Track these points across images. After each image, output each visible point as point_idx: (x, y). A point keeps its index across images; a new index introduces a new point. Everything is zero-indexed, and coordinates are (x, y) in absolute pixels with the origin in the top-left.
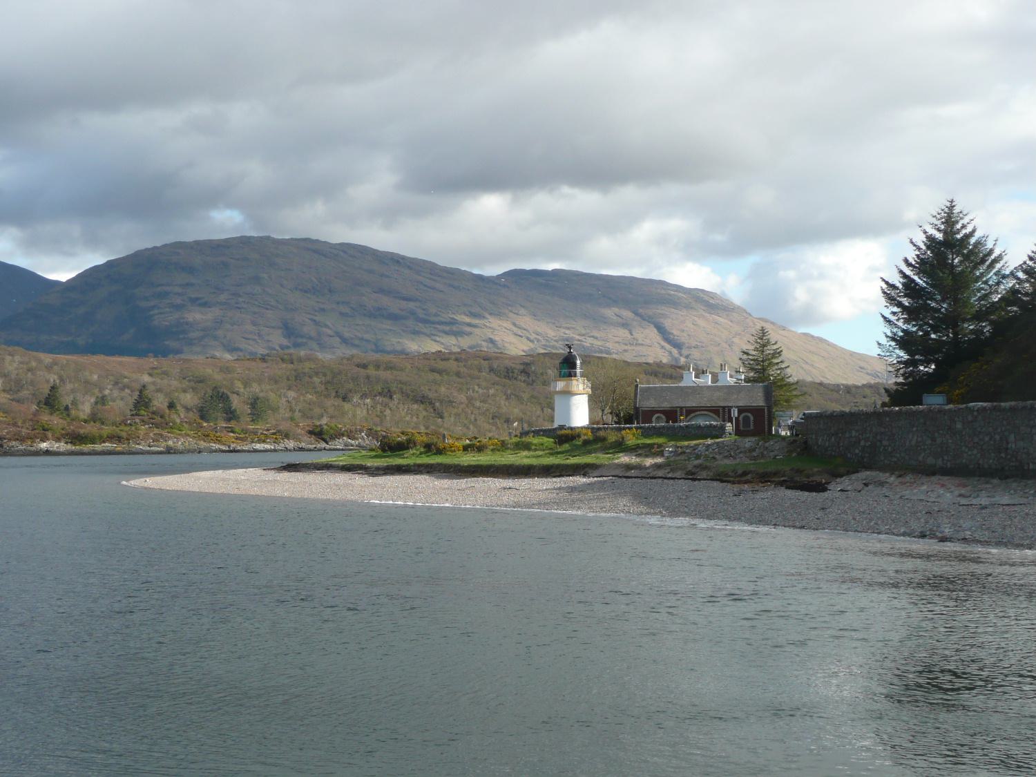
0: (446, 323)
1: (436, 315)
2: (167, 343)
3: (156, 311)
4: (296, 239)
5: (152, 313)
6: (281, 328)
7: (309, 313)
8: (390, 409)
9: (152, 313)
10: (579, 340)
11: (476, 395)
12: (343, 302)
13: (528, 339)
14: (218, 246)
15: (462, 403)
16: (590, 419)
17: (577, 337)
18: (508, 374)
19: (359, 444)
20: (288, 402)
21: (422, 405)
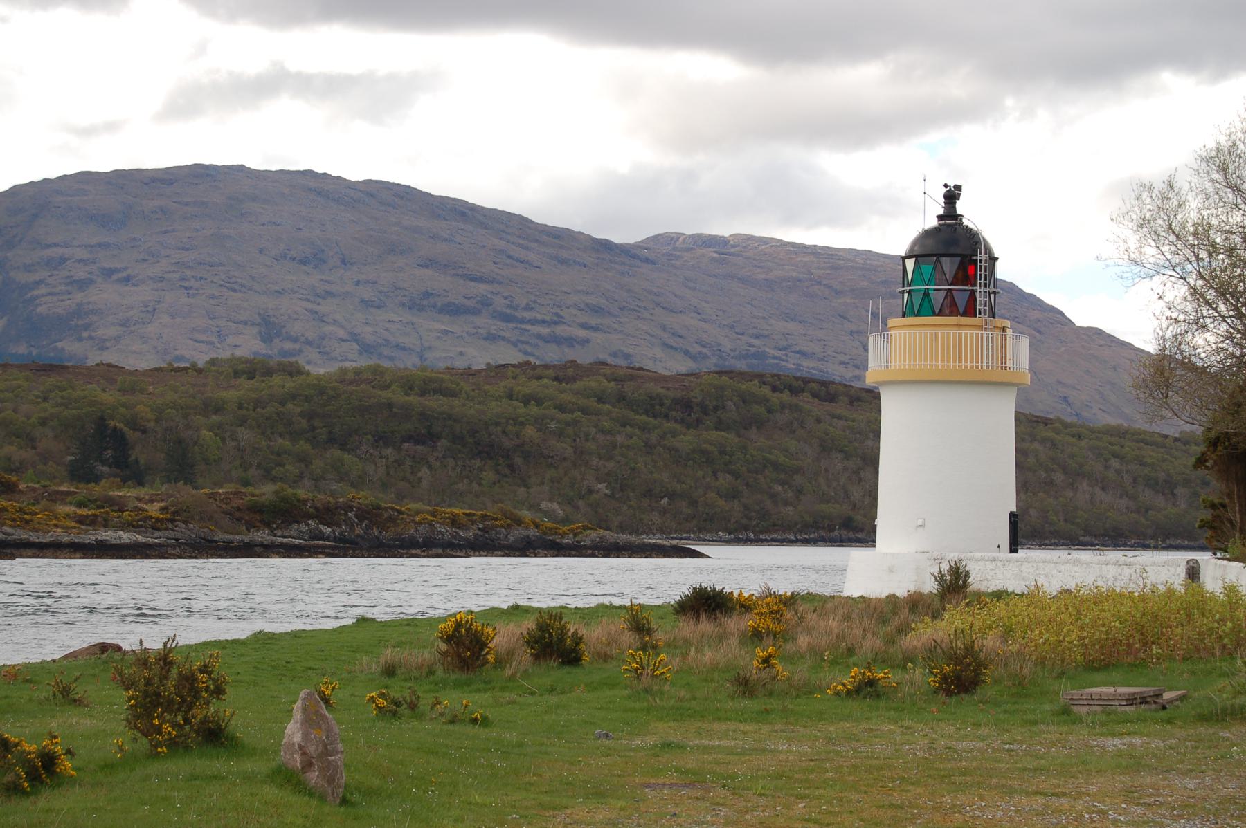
0: (544, 322)
1: (528, 308)
2: (59, 345)
3: (43, 290)
4: (289, 172)
5: (36, 292)
6: (259, 325)
7: (308, 300)
8: (430, 467)
9: (36, 292)
10: (775, 358)
11: (591, 446)
12: (367, 282)
13: (687, 353)
14: (154, 180)
15: (565, 459)
16: (1012, 288)
17: (772, 352)
18: (652, 406)
19: (341, 533)
20: (239, 449)
21: (489, 462)
